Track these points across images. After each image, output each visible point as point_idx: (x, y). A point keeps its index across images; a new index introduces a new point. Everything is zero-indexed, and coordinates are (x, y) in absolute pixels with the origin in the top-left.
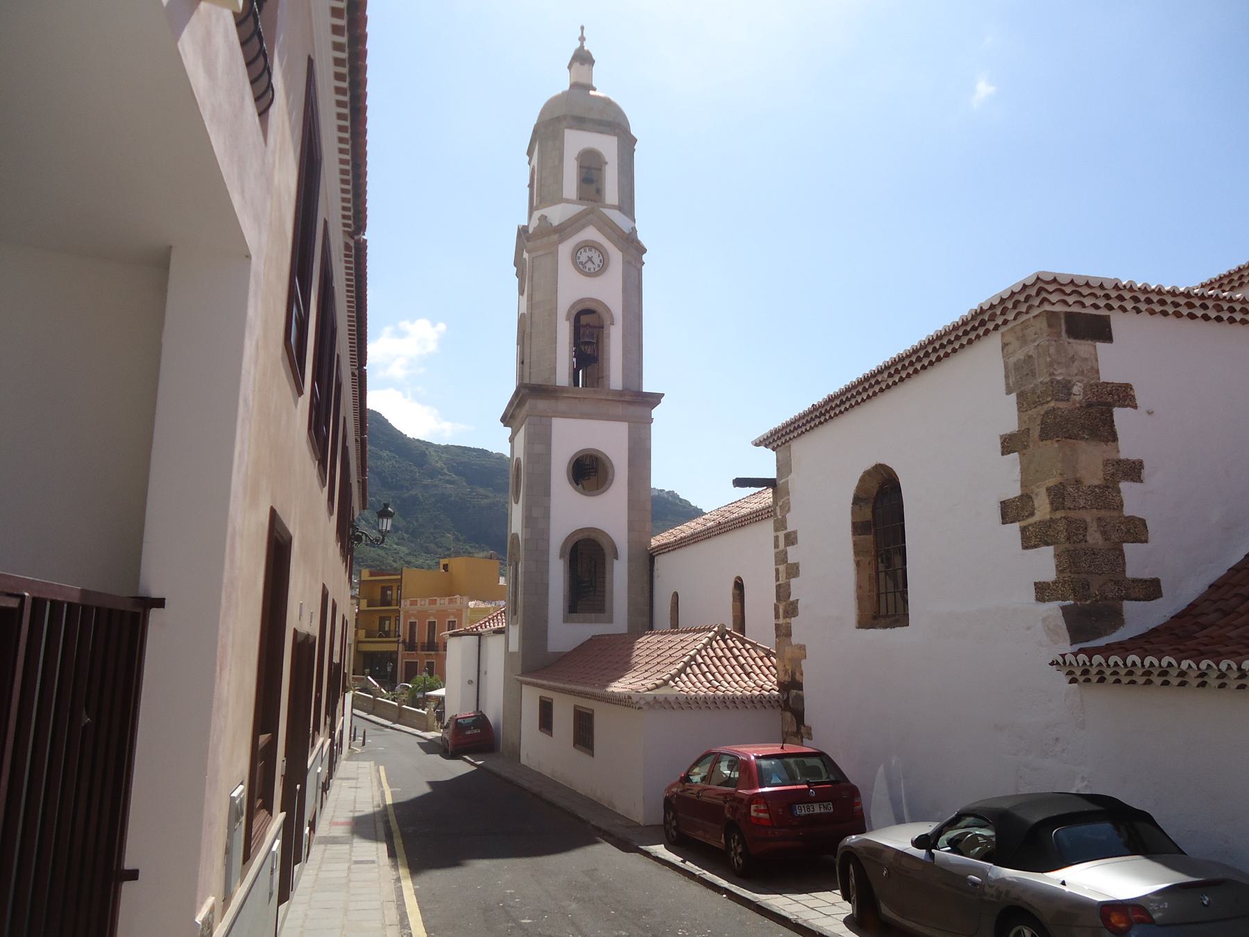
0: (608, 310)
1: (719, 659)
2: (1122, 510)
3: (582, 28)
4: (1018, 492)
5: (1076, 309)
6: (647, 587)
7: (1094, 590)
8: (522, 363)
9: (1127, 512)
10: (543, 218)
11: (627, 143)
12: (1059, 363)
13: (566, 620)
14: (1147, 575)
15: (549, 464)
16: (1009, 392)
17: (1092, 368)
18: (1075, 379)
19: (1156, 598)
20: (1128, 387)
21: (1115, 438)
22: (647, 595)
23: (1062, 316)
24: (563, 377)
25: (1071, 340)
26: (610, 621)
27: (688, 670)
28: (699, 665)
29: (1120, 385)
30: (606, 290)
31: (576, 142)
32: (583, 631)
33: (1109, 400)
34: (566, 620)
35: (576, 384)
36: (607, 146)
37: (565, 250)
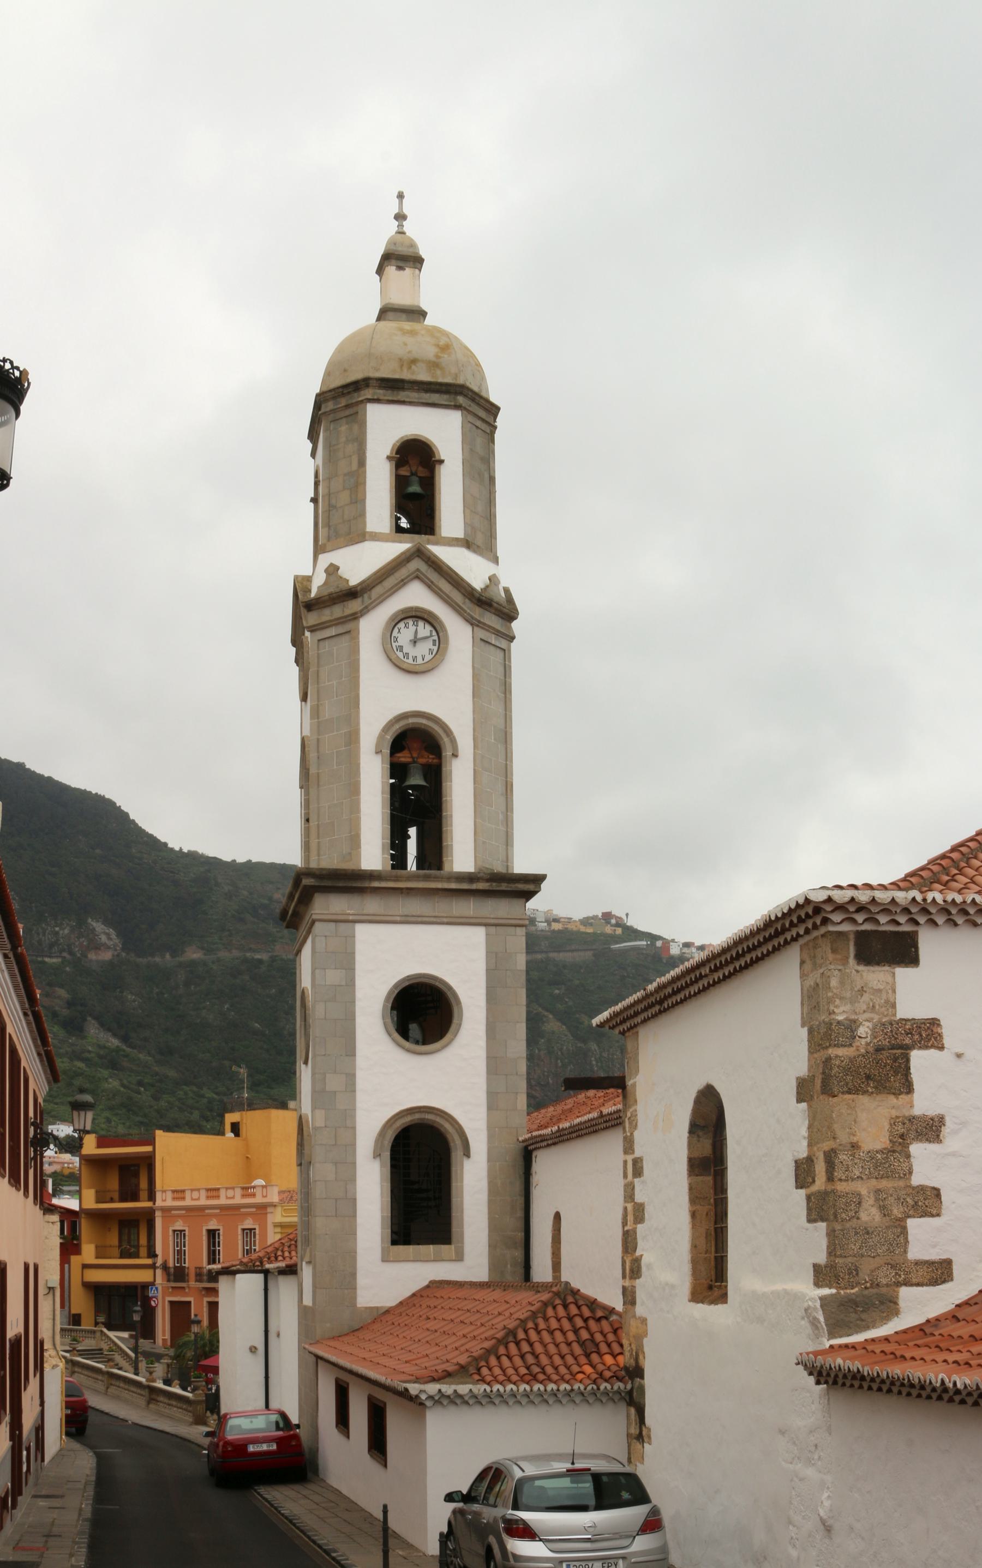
0: (448, 732)
1: (551, 1333)
2: (910, 1179)
3: (401, 196)
4: (805, 1155)
5: (868, 927)
6: (521, 1201)
7: (864, 1275)
8: (308, 820)
9: (916, 1180)
10: (332, 570)
11: (480, 412)
12: (841, 998)
13: (385, 1259)
14: (934, 1255)
15: (353, 1002)
16: (803, 1026)
17: (887, 1002)
18: (861, 1018)
19: (944, 1282)
20: (934, 1022)
21: (908, 1088)
22: (520, 1214)
23: (852, 937)
24: (372, 855)
25: (861, 968)
26: (459, 1257)
27: (502, 1350)
28: (517, 1343)
29: (924, 1022)
30: (446, 698)
31: (387, 425)
32: (415, 1271)
33: (908, 1041)
34: (385, 1259)
35: (399, 860)
36: (443, 429)
37: (371, 627)
